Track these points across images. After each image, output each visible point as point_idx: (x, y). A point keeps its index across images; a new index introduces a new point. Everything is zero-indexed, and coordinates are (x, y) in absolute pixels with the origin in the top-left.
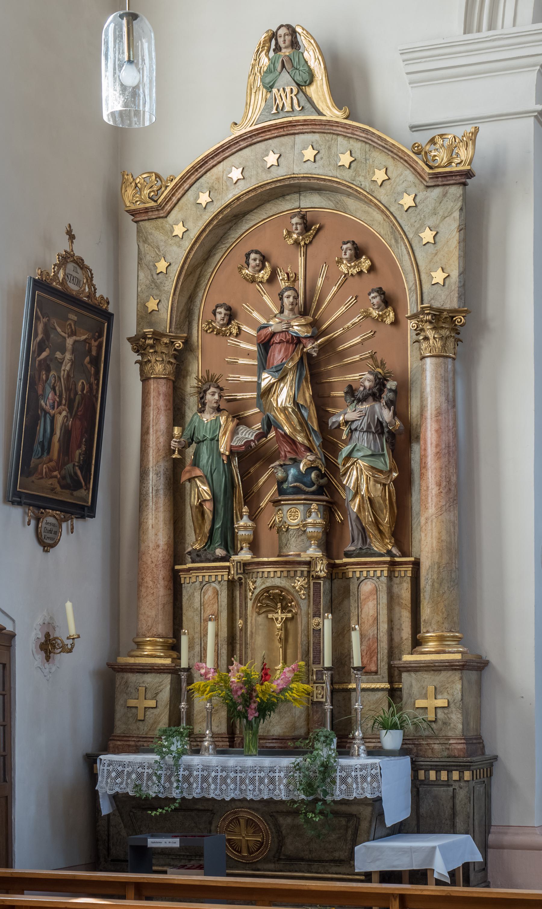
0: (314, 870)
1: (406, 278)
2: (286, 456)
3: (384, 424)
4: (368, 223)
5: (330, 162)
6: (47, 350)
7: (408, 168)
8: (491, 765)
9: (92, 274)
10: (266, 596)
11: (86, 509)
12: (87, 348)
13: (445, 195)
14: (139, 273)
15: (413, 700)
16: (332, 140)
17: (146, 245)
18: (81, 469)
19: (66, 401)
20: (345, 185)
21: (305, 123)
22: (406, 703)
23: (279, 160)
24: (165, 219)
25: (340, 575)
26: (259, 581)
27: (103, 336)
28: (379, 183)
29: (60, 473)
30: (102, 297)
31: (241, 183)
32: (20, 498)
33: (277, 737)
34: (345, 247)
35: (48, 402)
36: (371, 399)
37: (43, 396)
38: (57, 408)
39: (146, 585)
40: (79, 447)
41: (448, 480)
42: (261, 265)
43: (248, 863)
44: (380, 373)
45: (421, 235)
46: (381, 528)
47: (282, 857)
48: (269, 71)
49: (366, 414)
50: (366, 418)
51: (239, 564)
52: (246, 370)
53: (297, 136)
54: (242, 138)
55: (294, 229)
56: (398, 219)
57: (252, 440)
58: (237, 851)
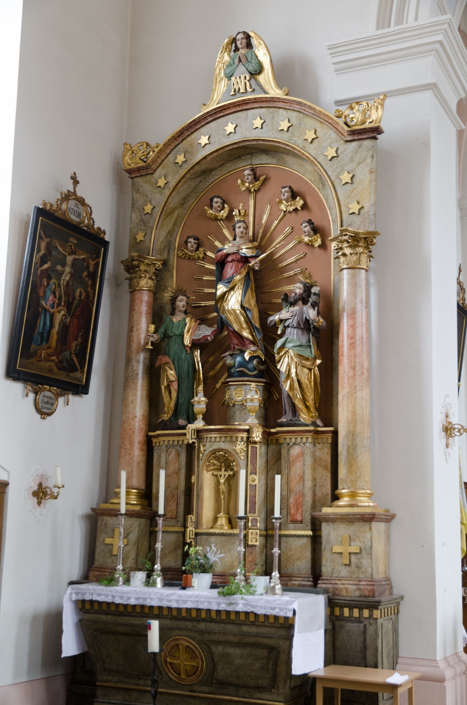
0: (241, 695)
1: (330, 212)
2: (234, 348)
3: (311, 322)
4: (302, 173)
5: (273, 127)
6: (49, 263)
7: (332, 129)
8: (398, 604)
9: (91, 211)
10: (213, 457)
11: (80, 387)
12: (85, 265)
13: (359, 147)
15: (331, 546)
16: (275, 111)
17: (138, 194)
18: (77, 356)
19: (65, 304)
20: (284, 144)
21: (256, 101)
22: (324, 549)
24: (152, 175)
25: (274, 442)
26: (208, 444)
27: (100, 257)
28: (310, 141)
29: (57, 358)
30: (99, 228)
32: (19, 375)
33: (218, 574)
34: (283, 190)
35: (48, 303)
36: (300, 303)
37: (44, 297)
38: (57, 307)
39: (125, 447)
40: (76, 339)
41: (361, 365)
42: (221, 206)
44: (308, 283)
45: (341, 177)
46: (308, 404)
47: (214, 681)
48: (229, 65)
49: (296, 314)
50: (296, 317)
51: (193, 431)
53: (249, 111)
54: (209, 114)
55: (246, 179)
56: (324, 166)
57: (208, 335)
58: (177, 674)
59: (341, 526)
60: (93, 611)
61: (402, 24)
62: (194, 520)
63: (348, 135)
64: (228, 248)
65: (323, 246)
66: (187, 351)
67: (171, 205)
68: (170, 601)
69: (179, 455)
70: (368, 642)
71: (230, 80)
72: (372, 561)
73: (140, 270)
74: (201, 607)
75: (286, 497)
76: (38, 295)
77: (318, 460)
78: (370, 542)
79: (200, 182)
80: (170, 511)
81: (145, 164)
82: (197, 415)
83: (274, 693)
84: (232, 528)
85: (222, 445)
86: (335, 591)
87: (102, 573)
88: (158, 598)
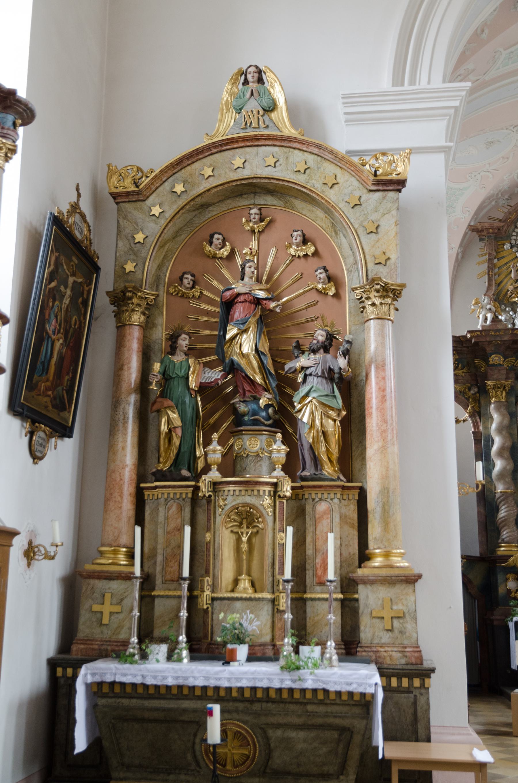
6: (56, 281)
7: (353, 176)
13: (384, 198)
14: (118, 242)
15: (369, 610)
16: (289, 152)
17: (125, 221)
21: (268, 138)
22: (363, 613)
23: (245, 164)
26: (230, 498)
29: (53, 393)
31: (211, 179)
32: (23, 409)
34: (295, 234)
36: (322, 351)
37: (49, 320)
40: (68, 374)
43: (232, 777)
50: (320, 365)
51: (209, 483)
52: (208, 325)
53: (260, 148)
57: (219, 379)
59: (380, 588)
60: (112, 695)
61: (415, 84)
62: (210, 583)
63: (373, 184)
64: (239, 288)
65: (337, 296)
66: (191, 395)
67: (165, 236)
68: (220, 679)
69: (181, 510)
70: (419, 714)
71: (239, 113)
72: (416, 626)
73: (133, 303)
74: (259, 684)
75: (312, 557)
76: (45, 318)
77: (343, 517)
78: (414, 606)
79: (195, 217)
80: (170, 573)
81: (137, 189)
82: (211, 465)
83: (342, 780)
84: (255, 591)
85: (248, 499)
86: (378, 659)
87: (89, 646)
88: (204, 677)
